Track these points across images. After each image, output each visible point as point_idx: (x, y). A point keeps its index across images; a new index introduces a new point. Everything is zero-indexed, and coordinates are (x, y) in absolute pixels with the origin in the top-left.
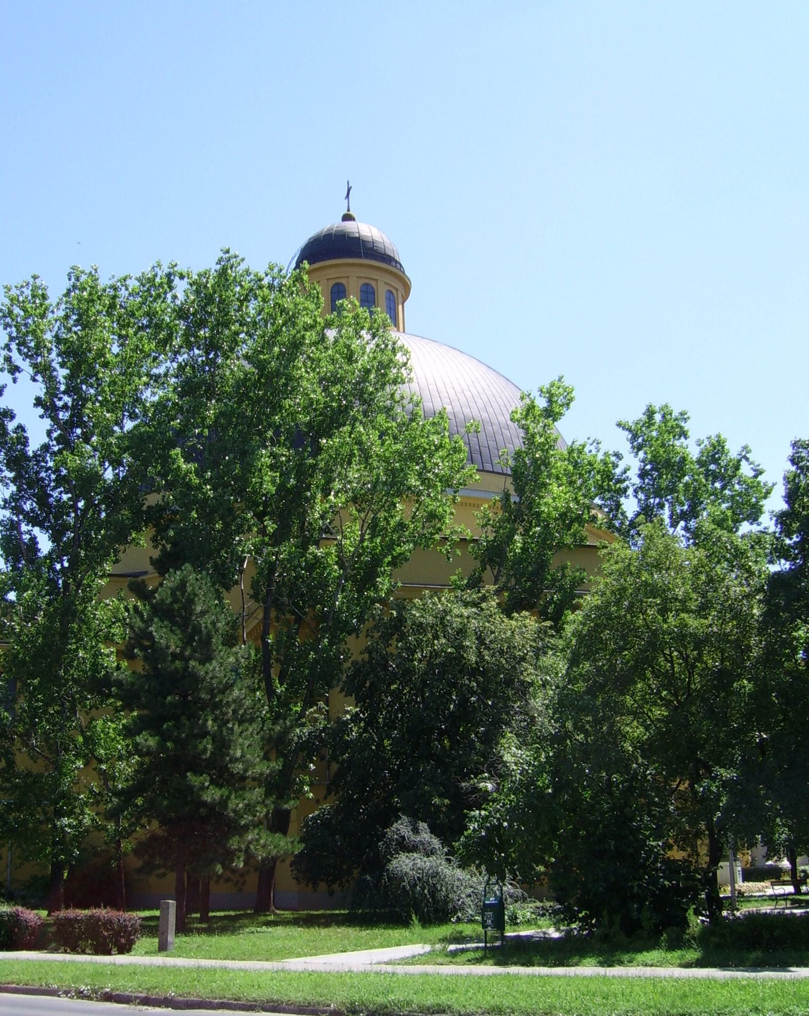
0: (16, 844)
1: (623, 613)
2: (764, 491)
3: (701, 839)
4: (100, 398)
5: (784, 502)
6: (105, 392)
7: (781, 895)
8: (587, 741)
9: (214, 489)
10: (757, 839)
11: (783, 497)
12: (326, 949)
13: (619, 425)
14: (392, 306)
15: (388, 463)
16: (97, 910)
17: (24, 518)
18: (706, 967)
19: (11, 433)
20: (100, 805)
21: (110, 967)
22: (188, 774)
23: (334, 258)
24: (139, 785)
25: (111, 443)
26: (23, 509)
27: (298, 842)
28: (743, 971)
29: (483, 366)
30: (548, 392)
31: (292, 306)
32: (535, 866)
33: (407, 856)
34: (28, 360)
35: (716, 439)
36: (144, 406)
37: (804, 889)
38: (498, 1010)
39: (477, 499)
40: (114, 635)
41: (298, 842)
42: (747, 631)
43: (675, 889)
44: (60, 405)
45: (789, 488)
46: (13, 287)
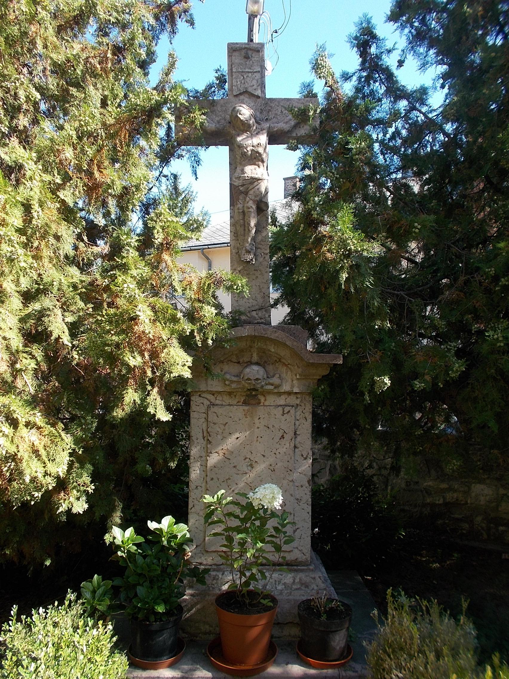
2: (267, 574)
3: (37, 331)
4: (84, 426)
5: (389, 9)
9: (369, 425)
10: (395, 592)
11: (424, 85)
12: (176, 488)
13: (197, 178)
14: (240, 230)
15: (359, 272)
16: (361, 421)
17: (454, 191)
19: (163, 124)
20: (74, 251)
26: (293, 226)
30: (164, 569)
32: (117, 516)
33: (265, 488)
34: (160, 37)
35: (16, 348)
36: (192, 304)
37: (101, 677)
38: (158, 677)
41: (97, 246)
45: (217, 128)
46: (438, 88)
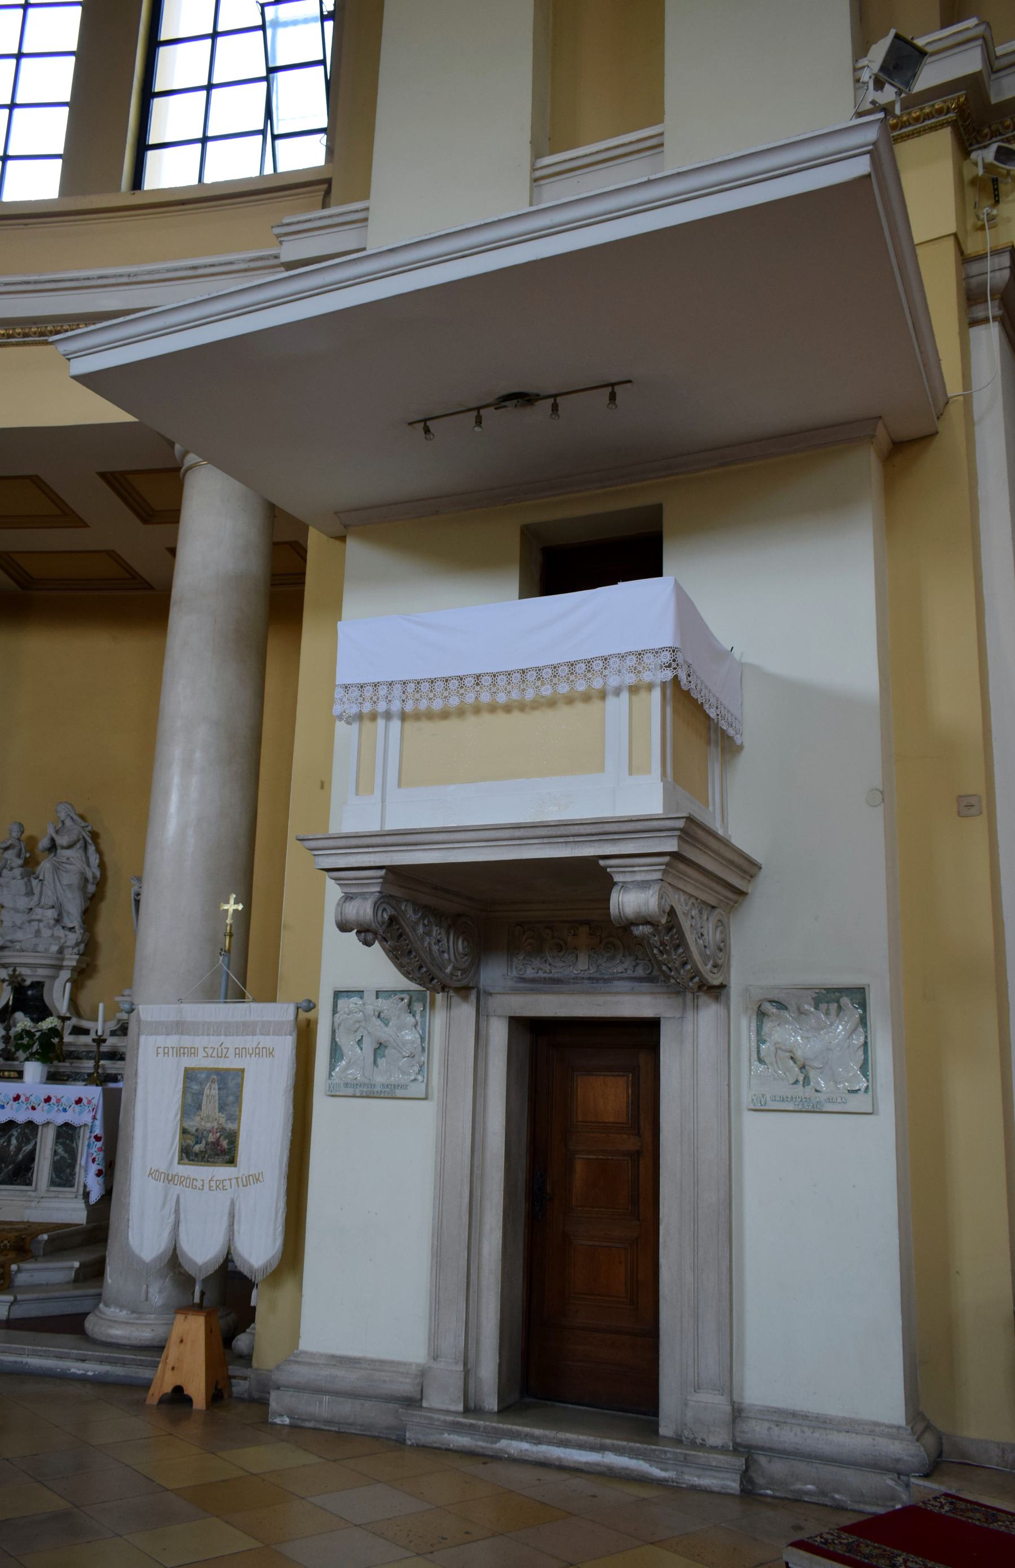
0: (952, 115)
1: (701, 942)
6: (208, 1122)
7: (73, 1153)
8: (574, 930)
18: (889, 33)
21: (882, 1428)
22: (234, 896)
23: (132, 81)
24: (822, 1029)
25: (987, 167)
27: (71, 1034)
28: (508, 1439)
29: (945, 239)
31: (53, 328)
39: (471, 1429)
40: (9, 975)
41: (71, 1034)
42: (640, 659)
43: (957, 103)
44: (118, 1333)
